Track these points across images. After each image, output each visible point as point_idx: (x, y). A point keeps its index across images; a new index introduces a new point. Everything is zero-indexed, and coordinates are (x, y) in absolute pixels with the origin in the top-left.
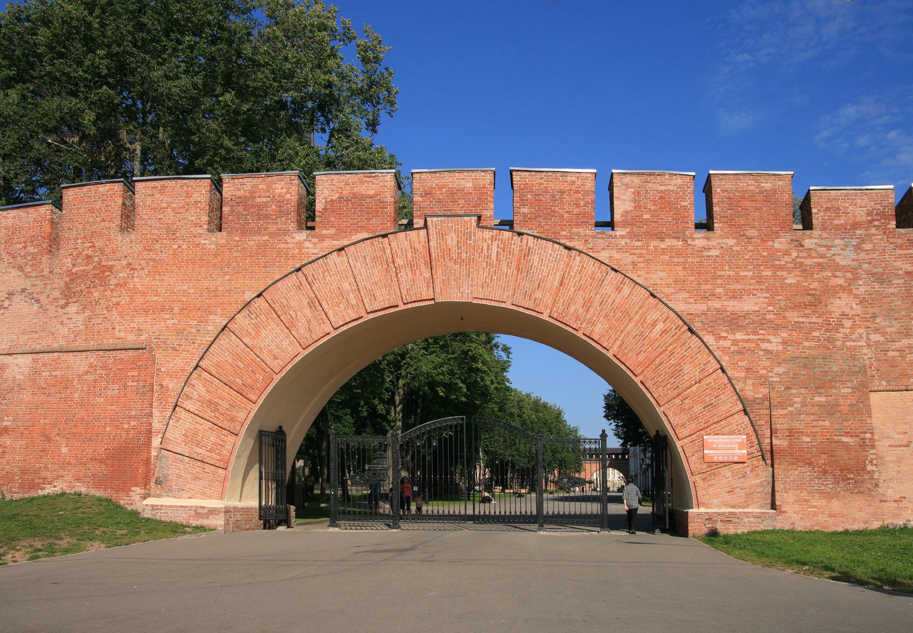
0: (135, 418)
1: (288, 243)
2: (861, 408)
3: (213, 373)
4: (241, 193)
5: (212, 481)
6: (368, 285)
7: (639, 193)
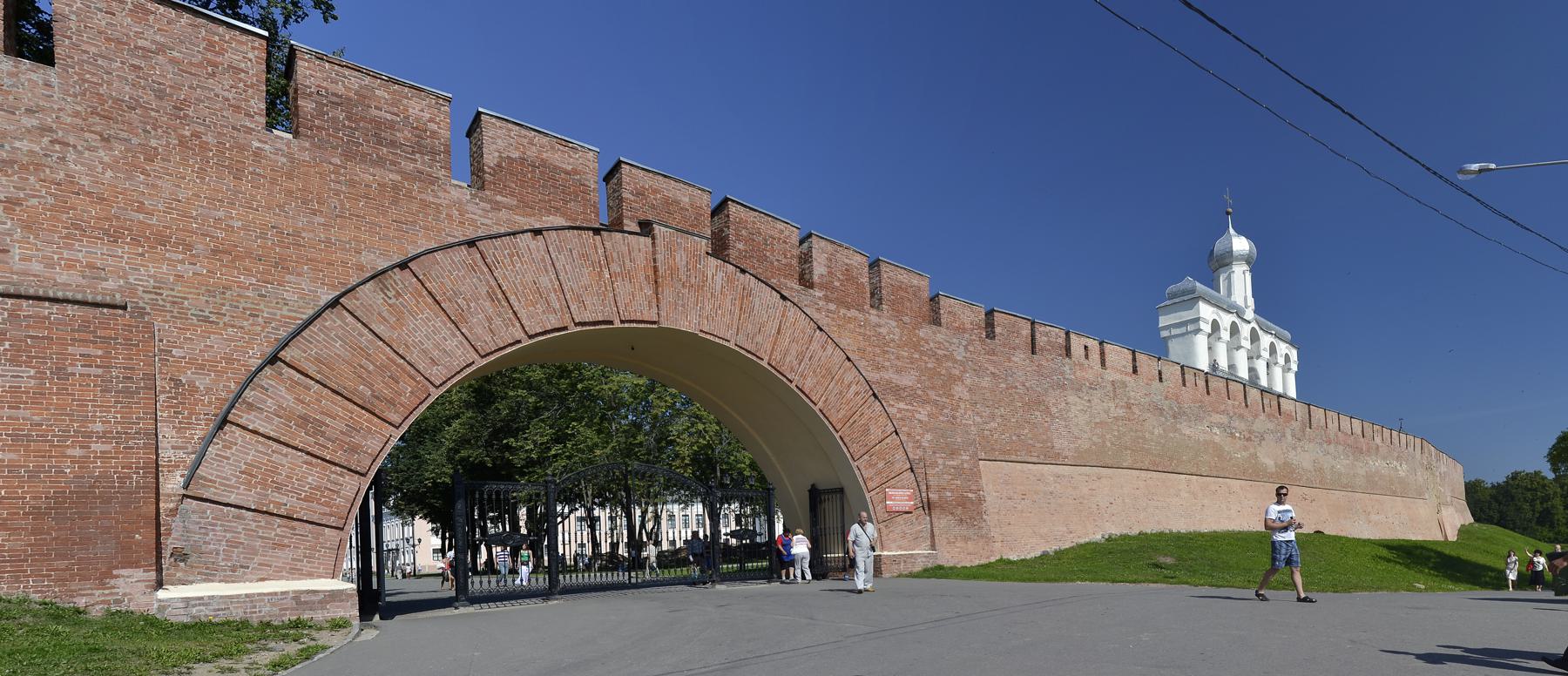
0: (103, 437)
2: (976, 475)
4: (340, 89)
5: (313, 548)
6: (575, 287)
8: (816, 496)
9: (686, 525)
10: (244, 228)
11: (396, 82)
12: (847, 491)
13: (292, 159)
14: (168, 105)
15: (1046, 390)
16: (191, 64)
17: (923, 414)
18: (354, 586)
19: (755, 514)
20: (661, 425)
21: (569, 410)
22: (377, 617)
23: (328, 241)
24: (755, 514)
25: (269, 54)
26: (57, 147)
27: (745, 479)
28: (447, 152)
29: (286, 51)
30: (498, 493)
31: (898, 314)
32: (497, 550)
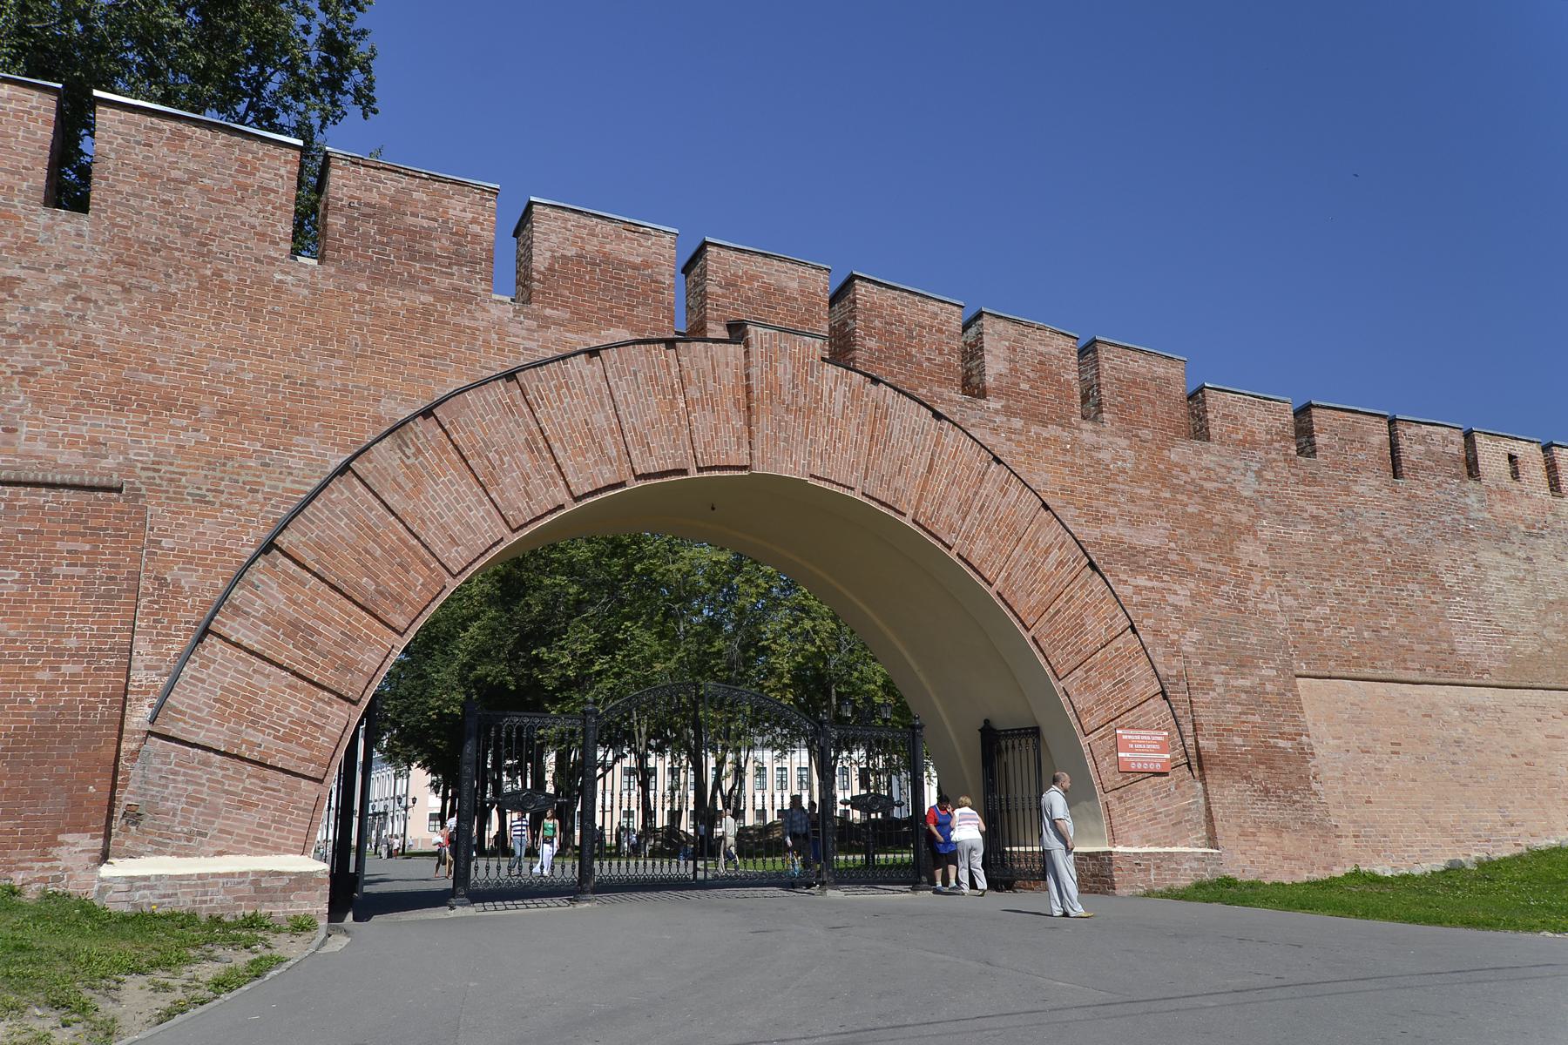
0: (76, 655)
1: (475, 319)
2: (1292, 705)
3: (309, 563)
4: (374, 197)
6: (638, 424)
8: (992, 740)
9: (783, 785)
10: (256, 381)
11: (437, 179)
12: (1046, 733)
13: (313, 289)
14: (192, 242)
15: (1429, 543)
16: (221, 190)
17: (1181, 594)
18: (326, 867)
19: (890, 769)
20: (749, 623)
21: (622, 603)
22: (350, 916)
23: (345, 389)
24: (890, 769)
25: (302, 166)
26: (79, 304)
27: (875, 710)
28: (490, 259)
29: (320, 159)
30: (520, 730)
31: (1129, 425)
32: (512, 817)
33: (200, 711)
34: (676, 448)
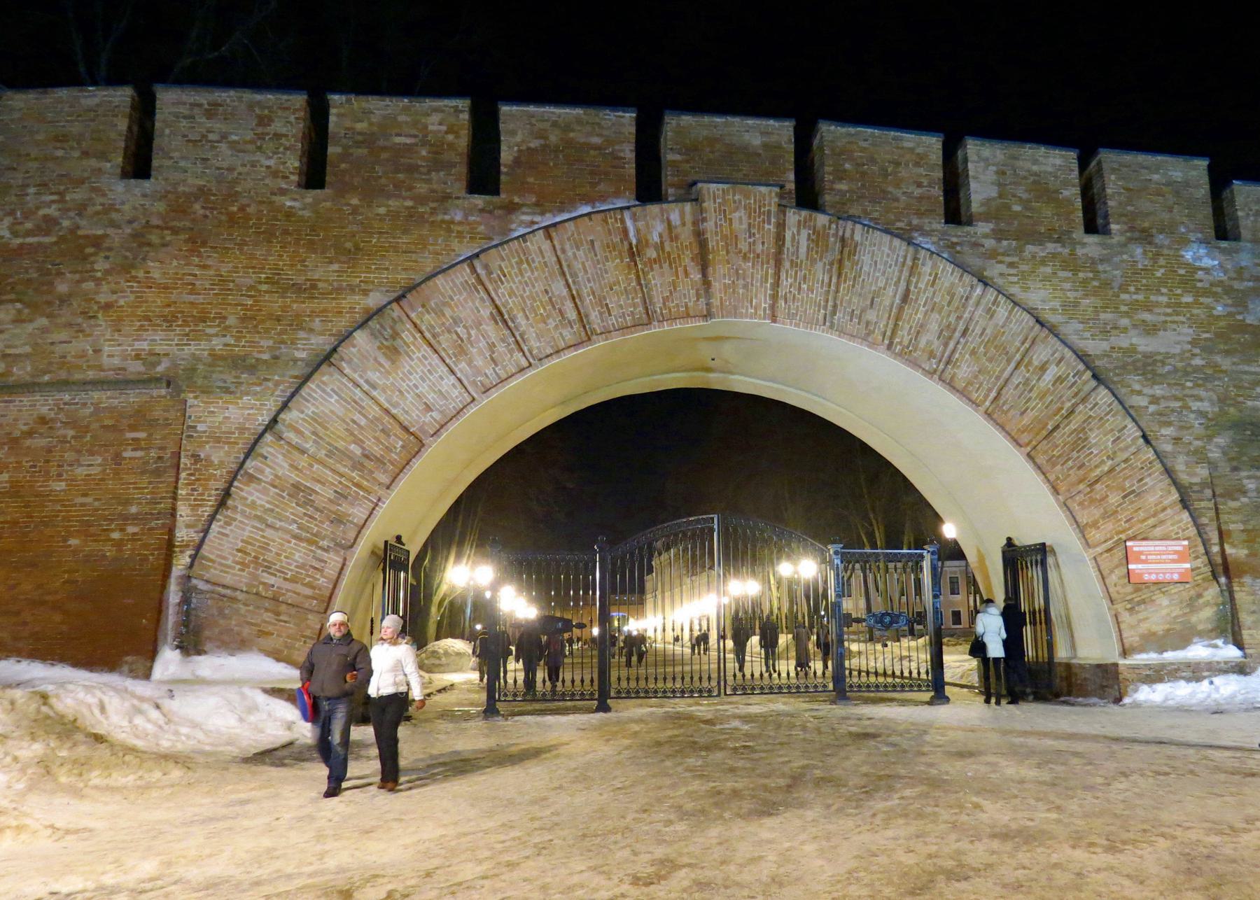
0: (135, 518)
7: (1004, 173)
16: (246, 142)
33: (225, 558)
34: (635, 306)
